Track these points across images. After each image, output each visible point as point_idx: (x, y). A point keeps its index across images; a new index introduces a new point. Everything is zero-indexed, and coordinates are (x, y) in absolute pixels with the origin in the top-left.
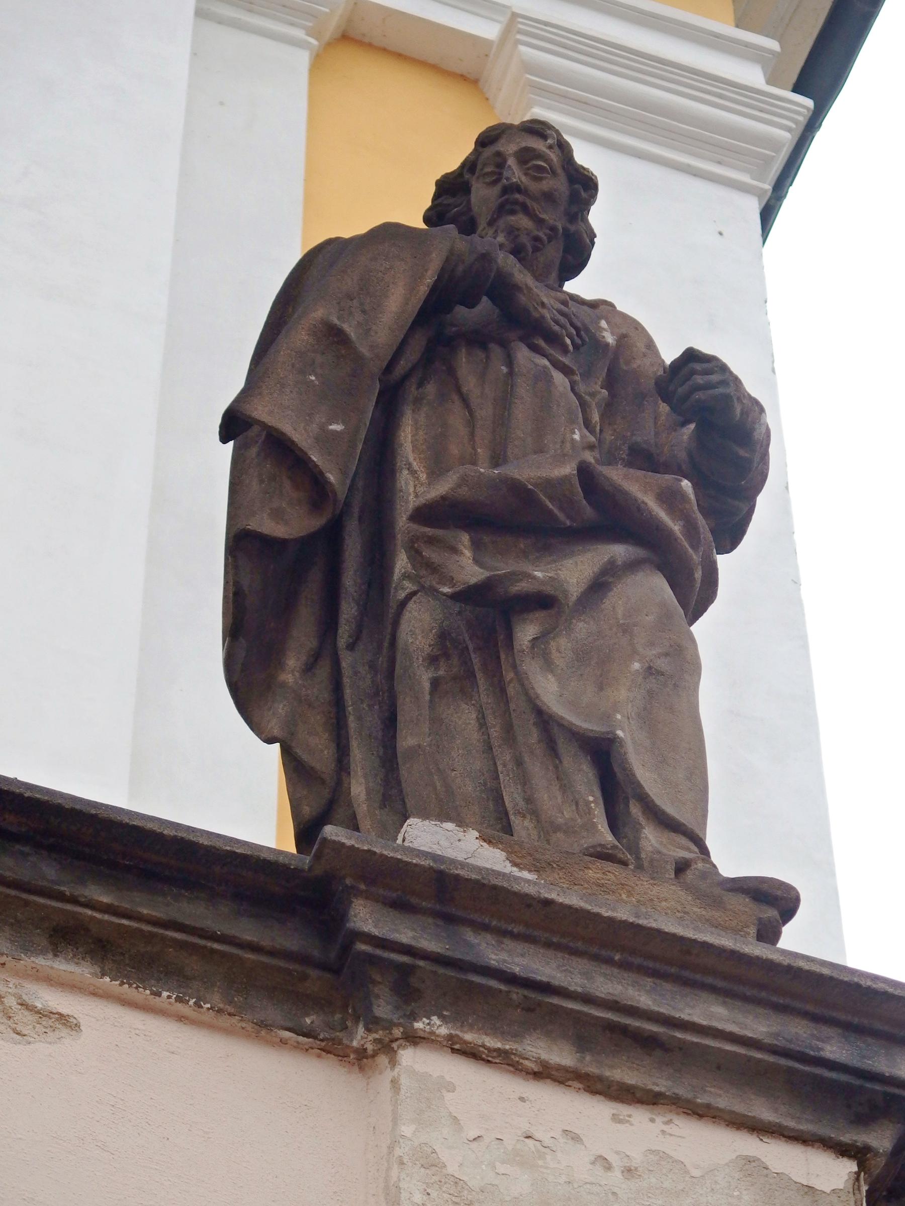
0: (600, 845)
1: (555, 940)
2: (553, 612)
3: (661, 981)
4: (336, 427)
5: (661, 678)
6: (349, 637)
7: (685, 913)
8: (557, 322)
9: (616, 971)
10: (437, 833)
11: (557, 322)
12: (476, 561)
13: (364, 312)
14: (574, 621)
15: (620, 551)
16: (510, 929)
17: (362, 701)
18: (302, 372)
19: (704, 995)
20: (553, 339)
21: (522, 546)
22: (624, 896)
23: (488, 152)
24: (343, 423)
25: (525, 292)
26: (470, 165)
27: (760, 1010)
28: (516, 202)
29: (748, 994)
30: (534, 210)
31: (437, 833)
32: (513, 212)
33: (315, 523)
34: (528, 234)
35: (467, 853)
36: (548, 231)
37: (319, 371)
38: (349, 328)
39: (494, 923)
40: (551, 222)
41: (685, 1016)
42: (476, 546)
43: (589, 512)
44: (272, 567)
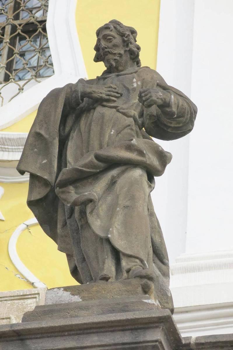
0: (102, 275)
1: (49, 335)
2: (92, 203)
3: (79, 335)
4: (44, 161)
5: (128, 208)
6: (68, 215)
7: (120, 291)
8: (108, 95)
9: (67, 337)
10: (52, 293)
11: (108, 95)
12: (76, 193)
13: (46, 123)
14: (107, 198)
15: (114, 172)
16: (37, 337)
17: (74, 233)
18: (32, 150)
19: (92, 335)
20: (108, 101)
21: (90, 181)
22: (103, 292)
23: (101, 37)
24: (47, 159)
25: (93, 93)
26: (99, 41)
27: (108, 334)
28: (106, 52)
29: (103, 331)
30: (112, 52)
31: (52, 293)
32: (107, 55)
33: (48, 189)
34: (112, 59)
35: (59, 297)
36: (118, 55)
37: (37, 147)
38: (43, 132)
39: (33, 337)
40: (118, 52)
41: (85, 345)
42: (76, 188)
43: (101, 165)
44: (44, 204)
